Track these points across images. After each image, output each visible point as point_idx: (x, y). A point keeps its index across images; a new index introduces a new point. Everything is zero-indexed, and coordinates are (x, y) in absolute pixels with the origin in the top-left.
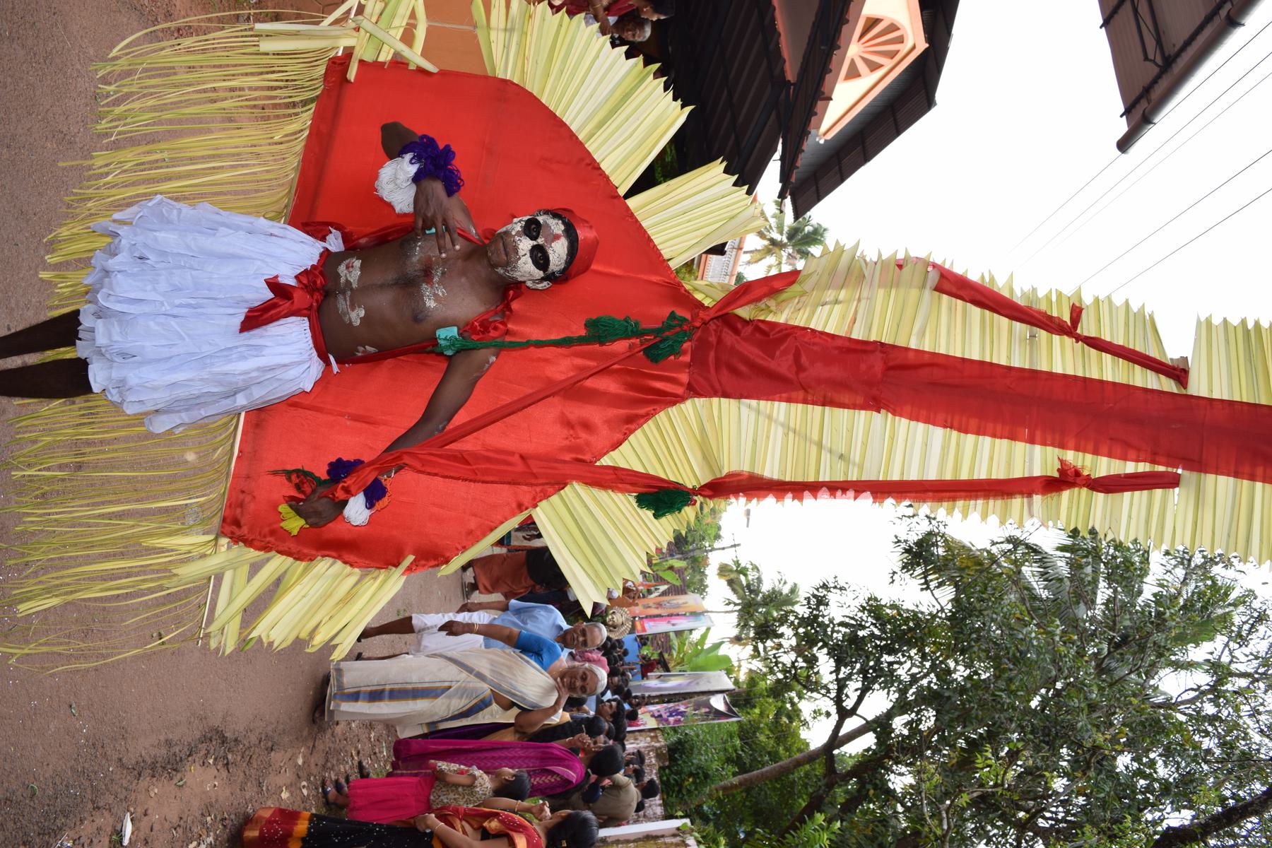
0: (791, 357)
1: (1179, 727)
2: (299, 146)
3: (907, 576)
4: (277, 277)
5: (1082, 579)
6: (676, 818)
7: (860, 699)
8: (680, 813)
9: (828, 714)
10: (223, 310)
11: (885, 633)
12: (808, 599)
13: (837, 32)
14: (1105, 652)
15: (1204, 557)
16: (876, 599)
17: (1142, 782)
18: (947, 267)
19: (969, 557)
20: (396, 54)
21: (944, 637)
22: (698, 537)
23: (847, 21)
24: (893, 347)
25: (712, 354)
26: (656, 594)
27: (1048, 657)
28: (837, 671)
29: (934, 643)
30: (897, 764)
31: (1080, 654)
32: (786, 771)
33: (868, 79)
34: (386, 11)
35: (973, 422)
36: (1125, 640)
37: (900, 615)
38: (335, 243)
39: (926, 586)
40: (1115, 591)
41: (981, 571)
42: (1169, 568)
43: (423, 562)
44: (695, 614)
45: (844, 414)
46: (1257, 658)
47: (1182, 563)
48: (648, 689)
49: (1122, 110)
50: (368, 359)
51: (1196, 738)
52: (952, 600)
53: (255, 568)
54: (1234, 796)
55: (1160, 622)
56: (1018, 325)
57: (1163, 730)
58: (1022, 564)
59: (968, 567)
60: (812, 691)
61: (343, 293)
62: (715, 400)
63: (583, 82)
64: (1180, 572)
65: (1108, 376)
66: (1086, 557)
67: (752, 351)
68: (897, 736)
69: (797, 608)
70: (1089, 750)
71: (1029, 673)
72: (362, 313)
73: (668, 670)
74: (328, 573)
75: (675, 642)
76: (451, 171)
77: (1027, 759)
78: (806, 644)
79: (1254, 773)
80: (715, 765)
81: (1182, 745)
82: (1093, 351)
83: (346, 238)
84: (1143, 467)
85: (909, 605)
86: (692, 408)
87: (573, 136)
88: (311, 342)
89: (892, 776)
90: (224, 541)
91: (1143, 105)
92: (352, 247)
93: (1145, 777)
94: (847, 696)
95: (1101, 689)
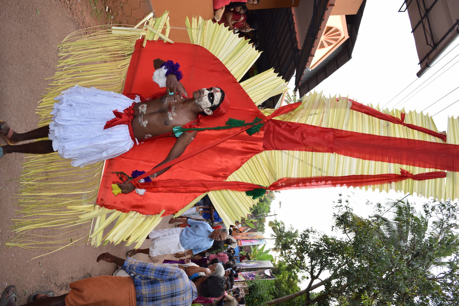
0: (300, 135)
2: (126, 69)
3: (338, 228)
4: (117, 110)
5: (402, 231)
9: (308, 278)
10: (98, 123)
11: (329, 248)
12: (301, 235)
13: (317, 33)
14: (410, 258)
15: (447, 224)
16: (326, 236)
18: (355, 100)
19: (361, 222)
20: (160, 38)
22: (262, 211)
23: (320, 29)
24: (337, 130)
25: (271, 135)
26: (246, 231)
28: (311, 262)
29: (347, 253)
30: (333, 296)
31: (401, 259)
33: (328, 48)
34: (156, 27)
35: (367, 156)
36: (418, 254)
37: (335, 242)
39: (345, 232)
40: (414, 236)
41: (365, 227)
44: (260, 239)
45: (320, 154)
48: (242, 266)
51: (444, 292)
52: (354, 237)
53: (108, 216)
55: (431, 248)
56: (382, 121)
57: (432, 288)
58: (380, 225)
59: (360, 226)
60: (302, 269)
61: (141, 115)
62: (273, 151)
64: (439, 230)
65: (417, 138)
66: (404, 223)
67: (287, 134)
68: (333, 287)
69: (297, 238)
71: (382, 265)
72: (147, 122)
75: (252, 249)
77: (380, 297)
78: (300, 252)
80: (266, 295)
82: (410, 129)
83: (141, 98)
84: (432, 170)
85: (338, 239)
86: (265, 154)
89: (331, 302)
90: (98, 206)
91: (426, 60)
92: (143, 101)
94: (315, 271)
95: (408, 272)
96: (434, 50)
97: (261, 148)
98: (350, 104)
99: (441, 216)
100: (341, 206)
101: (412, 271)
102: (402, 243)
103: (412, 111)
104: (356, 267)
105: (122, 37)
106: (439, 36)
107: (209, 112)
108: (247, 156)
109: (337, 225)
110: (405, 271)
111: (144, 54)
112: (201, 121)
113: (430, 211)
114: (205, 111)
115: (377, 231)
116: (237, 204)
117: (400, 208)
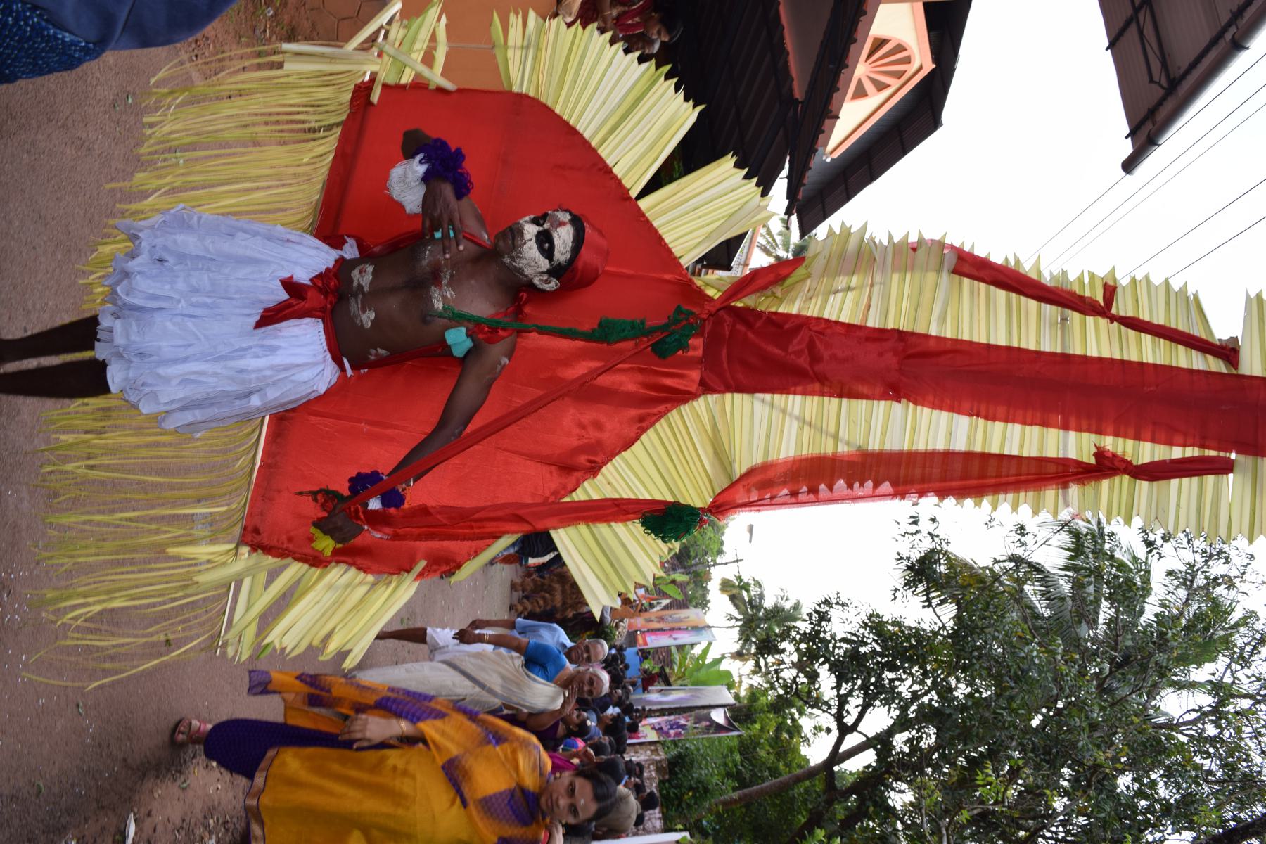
1: (1180, 747)
3: (909, 593)
5: (1084, 599)
6: (676, 831)
7: (861, 716)
8: (680, 826)
9: (829, 730)
10: (238, 311)
12: (810, 615)
13: (845, 51)
14: (1107, 671)
15: (1206, 578)
16: (878, 615)
17: (1143, 803)
18: (966, 249)
20: (418, 75)
21: (945, 655)
22: (700, 552)
23: (855, 41)
24: (913, 334)
26: (658, 608)
27: (1049, 676)
28: (838, 687)
29: (936, 660)
30: (896, 780)
31: (1082, 673)
32: (786, 787)
34: (409, 48)
35: (1001, 410)
36: (1127, 660)
37: (903, 632)
38: (350, 251)
40: (1117, 611)
42: (1171, 589)
43: (435, 567)
44: (697, 629)
45: (862, 405)
46: (1259, 679)
47: (1184, 584)
48: (650, 702)
49: (1128, 131)
50: (380, 363)
51: (1197, 760)
53: (273, 575)
54: (1235, 818)
55: (1162, 642)
56: (1048, 309)
59: (970, 585)
60: (812, 707)
61: (356, 296)
62: (728, 396)
63: (596, 90)
64: (1182, 593)
65: (1148, 358)
68: (898, 754)
69: (798, 624)
70: (1090, 768)
71: (1030, 692)
72: (373, 316)
73: (669, 684)
74: (341, 579)
75: (677, 657)
76: (462, 174)
77: (1028, 777)
78: (805, 664)
79: (1255, 795)
80: (715, 780)
81: (1183, 766)
82: (1131, 333)
84: (1191, 452)
85: (910, 622)
86: (704, 405)
87: (586, 143)
88: (325, 344)
89: (892, 794)
90: (245, 550)
91: (1149, 126)
92: (366, 255)
93: (1146, 797)
94: (848, 712)
95: (1102, 709)
96: (1169, 99)
97: (693, 388)
98: (950, 260)
99: (1188, 556)
100: (917, 532)
101: (1112, 705)
102: (1085, 632)
103: (1138, 278)
104: (961, 697)
105: (315, 76)
106: (1182, 59)
107: (547, 282)
108: (655, 411)
109: (906, 585)
110: (1092, 705)
111: (375, 121)
112: (527, 310)
113: (1159, 542)
114: (536, 281)
115: (1016, 600)
116: (624, 546)
117: (1076, 535)
